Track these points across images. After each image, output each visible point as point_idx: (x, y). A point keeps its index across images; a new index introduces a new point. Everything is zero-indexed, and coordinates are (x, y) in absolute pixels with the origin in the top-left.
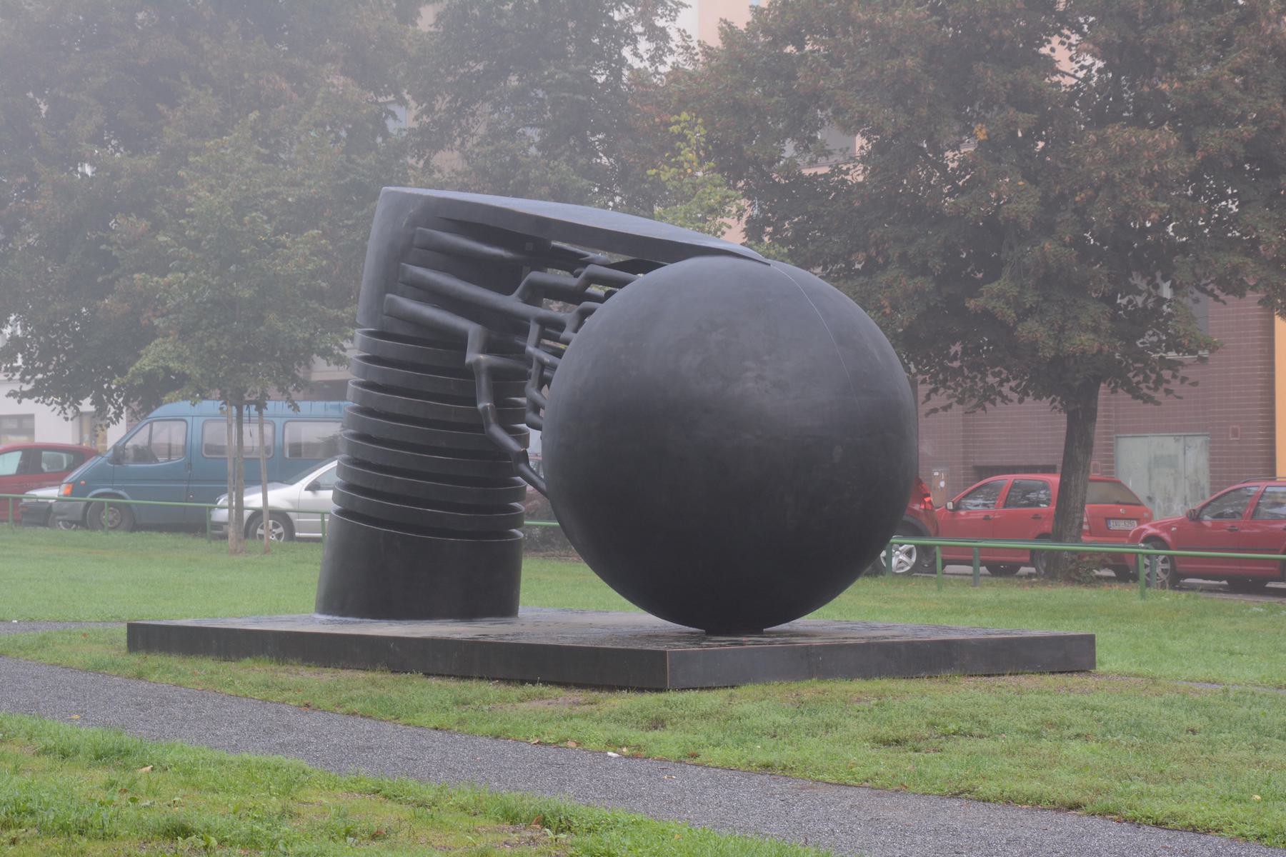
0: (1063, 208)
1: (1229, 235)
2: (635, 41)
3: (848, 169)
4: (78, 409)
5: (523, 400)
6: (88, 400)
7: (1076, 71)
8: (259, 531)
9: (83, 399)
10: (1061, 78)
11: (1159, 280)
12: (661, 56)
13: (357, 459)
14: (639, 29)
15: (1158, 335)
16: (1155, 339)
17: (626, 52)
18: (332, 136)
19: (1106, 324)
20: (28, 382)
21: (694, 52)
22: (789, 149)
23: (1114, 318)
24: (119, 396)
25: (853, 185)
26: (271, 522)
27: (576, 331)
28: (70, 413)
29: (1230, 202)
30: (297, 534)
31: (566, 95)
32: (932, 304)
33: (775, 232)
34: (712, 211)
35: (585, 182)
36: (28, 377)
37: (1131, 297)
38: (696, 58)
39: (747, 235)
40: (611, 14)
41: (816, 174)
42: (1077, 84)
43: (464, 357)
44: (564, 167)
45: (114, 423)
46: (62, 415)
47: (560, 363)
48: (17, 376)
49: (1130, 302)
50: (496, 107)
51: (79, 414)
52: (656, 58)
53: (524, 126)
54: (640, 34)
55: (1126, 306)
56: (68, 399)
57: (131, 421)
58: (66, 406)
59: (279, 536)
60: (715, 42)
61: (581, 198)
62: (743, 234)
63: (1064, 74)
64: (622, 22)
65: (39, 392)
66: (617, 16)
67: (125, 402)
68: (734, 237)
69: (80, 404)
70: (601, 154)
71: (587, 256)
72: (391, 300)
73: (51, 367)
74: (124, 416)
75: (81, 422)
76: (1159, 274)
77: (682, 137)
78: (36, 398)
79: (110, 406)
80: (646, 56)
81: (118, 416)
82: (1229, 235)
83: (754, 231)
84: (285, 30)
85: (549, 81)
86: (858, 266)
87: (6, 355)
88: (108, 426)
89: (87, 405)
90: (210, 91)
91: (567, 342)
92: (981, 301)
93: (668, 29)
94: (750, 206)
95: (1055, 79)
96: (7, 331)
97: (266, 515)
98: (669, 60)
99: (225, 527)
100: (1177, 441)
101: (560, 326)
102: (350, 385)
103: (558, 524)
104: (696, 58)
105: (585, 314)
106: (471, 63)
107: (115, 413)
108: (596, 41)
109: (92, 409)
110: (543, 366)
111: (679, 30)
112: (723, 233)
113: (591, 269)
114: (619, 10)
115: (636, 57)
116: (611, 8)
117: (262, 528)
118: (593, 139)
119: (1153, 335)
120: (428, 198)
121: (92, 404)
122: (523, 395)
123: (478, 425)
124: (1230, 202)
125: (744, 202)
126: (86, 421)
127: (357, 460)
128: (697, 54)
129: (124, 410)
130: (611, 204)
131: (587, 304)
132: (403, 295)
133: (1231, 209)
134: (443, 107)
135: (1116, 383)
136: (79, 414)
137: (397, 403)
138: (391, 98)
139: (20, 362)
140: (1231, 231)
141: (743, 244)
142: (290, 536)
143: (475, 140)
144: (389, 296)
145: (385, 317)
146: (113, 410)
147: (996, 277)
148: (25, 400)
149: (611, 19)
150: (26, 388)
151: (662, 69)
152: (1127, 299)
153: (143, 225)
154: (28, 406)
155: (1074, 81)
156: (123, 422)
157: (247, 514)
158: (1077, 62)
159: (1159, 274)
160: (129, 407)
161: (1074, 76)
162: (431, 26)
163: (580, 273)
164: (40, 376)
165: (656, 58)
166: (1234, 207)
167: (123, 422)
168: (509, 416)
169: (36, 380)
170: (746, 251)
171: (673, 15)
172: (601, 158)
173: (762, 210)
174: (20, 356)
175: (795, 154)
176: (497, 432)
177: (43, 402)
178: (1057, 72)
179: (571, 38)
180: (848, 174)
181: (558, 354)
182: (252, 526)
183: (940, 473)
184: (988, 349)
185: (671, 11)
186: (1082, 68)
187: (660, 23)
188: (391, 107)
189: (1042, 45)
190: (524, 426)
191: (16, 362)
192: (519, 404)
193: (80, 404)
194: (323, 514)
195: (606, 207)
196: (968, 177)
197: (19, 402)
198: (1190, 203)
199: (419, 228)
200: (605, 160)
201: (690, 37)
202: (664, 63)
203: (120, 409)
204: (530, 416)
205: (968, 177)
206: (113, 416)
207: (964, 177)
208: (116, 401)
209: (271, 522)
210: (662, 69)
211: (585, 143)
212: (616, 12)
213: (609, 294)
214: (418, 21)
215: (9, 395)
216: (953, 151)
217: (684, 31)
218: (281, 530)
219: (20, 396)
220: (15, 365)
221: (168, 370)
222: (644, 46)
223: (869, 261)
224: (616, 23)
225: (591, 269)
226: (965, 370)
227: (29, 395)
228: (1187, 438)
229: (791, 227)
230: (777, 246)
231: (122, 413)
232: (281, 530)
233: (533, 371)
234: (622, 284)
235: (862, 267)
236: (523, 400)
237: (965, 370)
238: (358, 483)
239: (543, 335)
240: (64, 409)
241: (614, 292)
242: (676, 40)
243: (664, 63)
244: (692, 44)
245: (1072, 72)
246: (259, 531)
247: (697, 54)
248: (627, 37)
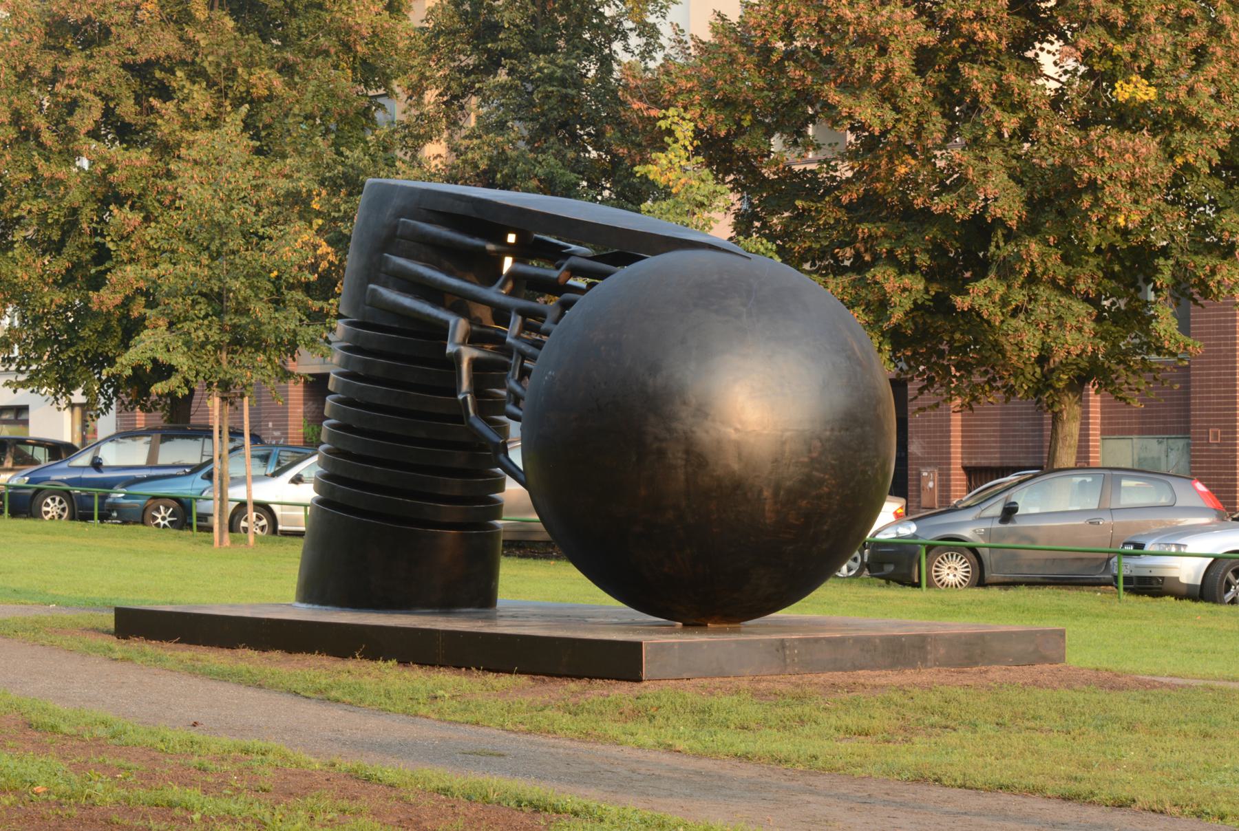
0: (1047, 209)
1: (1207, 240)
2: (625, 37)
3: (836, 165)
4: (70, 401)
5: (503, 393)
6: (80, 390)
7: (1060, 76)
8: (243, 524)
9: (74, 389)
10: (1046, 82)
11: (1141, 283)
12: (651, 51)
13: (338, 449)
14: (628, 24)
15: (1140, 337)
16: (1137, 341)
17: (617, 46)
18: (323, 128)
19: (1089, 325)
20: (23, 372)
21: (686, 46)
22: (777, 143)
23: (1099, 320)
24: (109, 387)
25: (841, 181)
26: (254, 514)
27: (556, 322)
28: (63, 402)
29: (1208, 208)
30: (280, 527)
31: (554, 89)
32: (919, 302)
33: (764, 225)
34: (701, 205)
35: (573, 177)
36: (23, 368)
37: (1114, 299)
38: (688, 52)
39: (735, 229)
40: (601, 10)
41: (805, 169)
42: (1061, 88)
43: (445, 346)
44: (552, 161)
45: (104, 414)
46: (55, 405)
47: (541, 354)
48: (14, 367)
49: (1113, 304)
50: (485, 100)
51: (72, 406)
52: (646, 54)
53: (514, 119)
54: (631, 30)
55: (1110, 308)
56: (61, 389)
57: (120, 412)
58: (58, 396)
59: (263, 528)
60: (707, 36)
61: (569, 191)
62: (731, 228)
63: (1048, 78)
64: (613, 18)
65: (34, 381)
66: (608, 12)
67: (115, 393)
68: (721, 228)
69: (72, 394)
70: (590, 148)
71: (569, 248)
72: (374, 290)
73: (45, 358)
74: (114, 406)
75: (72, 411)
76: (1141, 277)
77: (670, 132)
78: (31, 389)
79: (100, 397)
80: (637, 52)
81: (108, 406)
82: (1207, 240)
83: (743, 224)
84: (279, 26)
85: (538, 74)
86: (847, 263)
87: (5, 344)
88: (98, 416)
89: (78, 396)
90: (204, 85)
91: (547, 334)
92: (968, 300)
93: (658, 26)
94: (739, 200)
95: (1040, 82)
96: (7, 320)
97: (250, 508)
98: (659, 56)
99: (210, 518)
100: (1160, 443)
101: (540, 315)
102: (332, 375)
103: (536, 518)
104: (688, 52)
105: (566, 305)
106: (462, 57)
107: (105, 403)
108: (587, 36)
109: (83, 400)
110: (524, 356)
111: (672, 23)
112: (711, 228)
113: (573, 261)
114: (609, 6)
115: (624, 53)
116: (602, 4)
117: (246, 520)
118: (582, 132)
119: (1135, 337)
120: (413, 191)
121: (83, 394)
122: (503, 387)
123: (459, 415)
124: (1208, 208)
125: (733, 197)
126: (77, 410)
127: (337, 454)
128: (689, 48)
129: (114, 401)
130: (599, 198)
131: (568, 296)
132: (385, 286)
133: (1209, 215)
134: (432, 101)
135: (1100, 384)
136: (72, 406)
137: (376, 393)
138: (381, 91)
139: (16, 352)
140: (1208, 236)
141: (731, 239)
142: (274, 531)
143: (464, 132)
144: (372, 286)
145: (368, 308)
146: (102, 401)
147: (984, 276)
148: (20, 391)
149: (602, 14)
150: (22, 378)
151: (652, 65)
152: (1110, 300)
153: (137, 217)
154: (22, 397)
155: (1058, 85)
156: (113, 412)
157: (231, 506)
158: (1061, 67)
159: (1141, 277)
160: (118, 398)
161: (1058, 81)
162: (422, 21)
163: (562, 265)
164: (34, 367)
165: (646, 54)
166: (1211, 212)
167: (113, 412)
168: (488, 406)
169: (31, 371)
170: (731, 246)
171: (663, 11)
172: (589, 152)
173: (751, 205)
174: (16, 346)
175: (784, 149)
176: (479, 425)
177: (38, 392)
178: (1042, 75)
179: (562, 34)
180: (837, 171)
181: (538, 345)
182: (237, 518)
183: (929, 473)
184: (975, 348)
185: (661, 8)
186: (1066, 72)
187: (651, 19)
188: (381, 101)
189: (1027, 49)
190: (504, 418)
191: (13, 352)
192: (501, 397)
193: (72, 394)
194: (306, 506)
195: (594, 199)
196: (955, 176)
197: (15, 391)
198: (1170, 207)
199: (402, 219)
200: (594, 154)
201: (682, 31)
202: (653, 59)
203: (110, 399)
204: (510, 408)
205: (955, 176)
206: (103, 407)
207: (951, 176)
208: (107, 391)
209: (254, 514)
210: (652, 65)
211: (574, 137)
212: (606, 8)
213: (591, 285)
214: (410, 15)
215: (7, 384)
216: (941, 150)
217: (677, 25)
218: (264, 522)
219: (17, 386)
220: (11, 356)
221: (154, 361)
222: (634, 41)
223: (858, 256)
224: (606, 18)
225: (573, 261)
226: (953, 369)
227: (23, 385)
228: (1170, 441)
229: (780, 223)
230: (765, 241)
231: (112, 403)
232: (264, 522)
233: (514, 362)
234: (603, 275)
235: (851, 263)
236: (503, 393)
237: (953, 369)
238: (338, 473)
239: (525, 327)
240: (57, 399)
241: (596, 284)
242: (666, 32)
243: (653, 59)
244: (684, 39)
245: (1056, 77)
246: (243, 524)
247: (689, 48)
248: (617, 32)
